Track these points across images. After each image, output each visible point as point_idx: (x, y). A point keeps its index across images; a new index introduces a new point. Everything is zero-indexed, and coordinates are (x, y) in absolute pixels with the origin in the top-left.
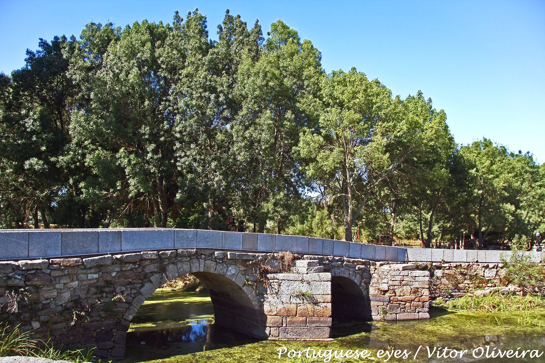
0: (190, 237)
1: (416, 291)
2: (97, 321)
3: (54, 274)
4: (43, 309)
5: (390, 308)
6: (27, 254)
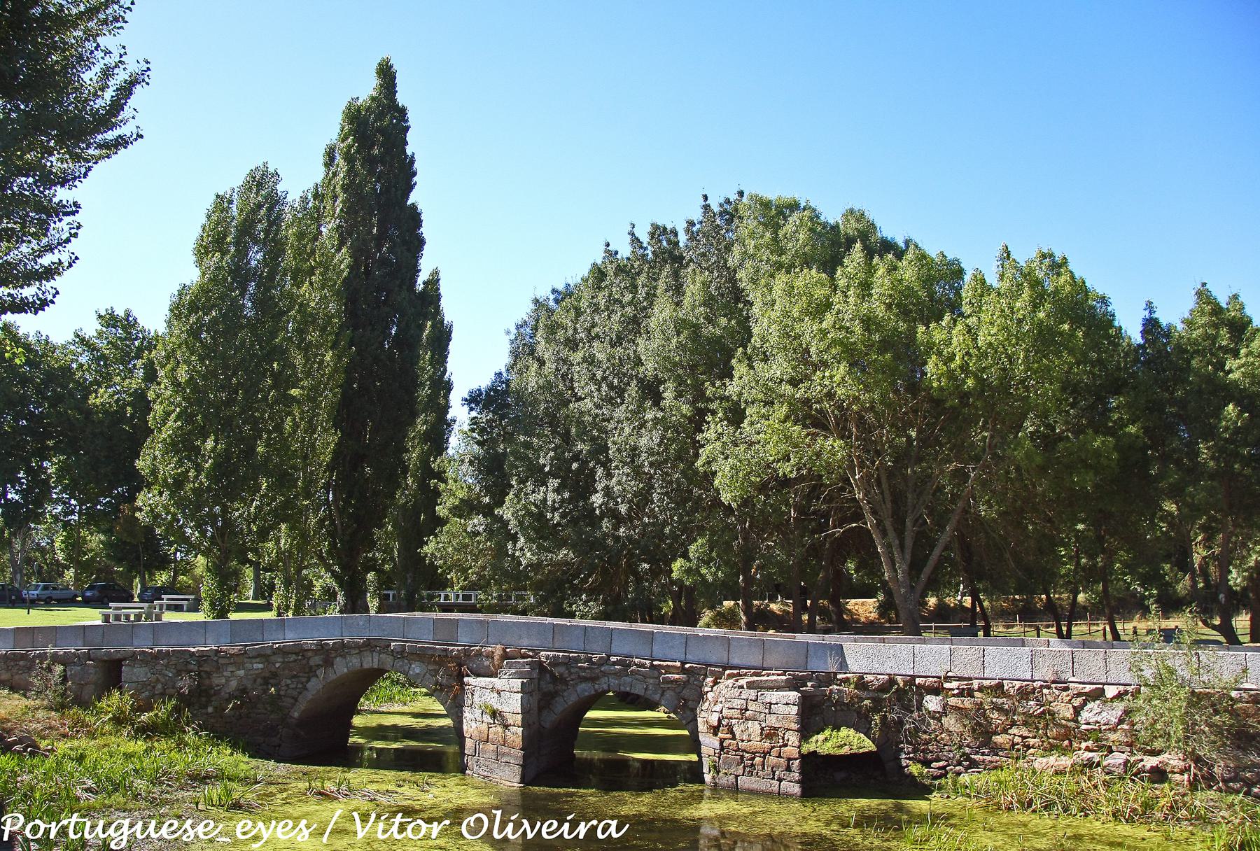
1: (770, 734)
3: (221, 661)
5: (724, 763)
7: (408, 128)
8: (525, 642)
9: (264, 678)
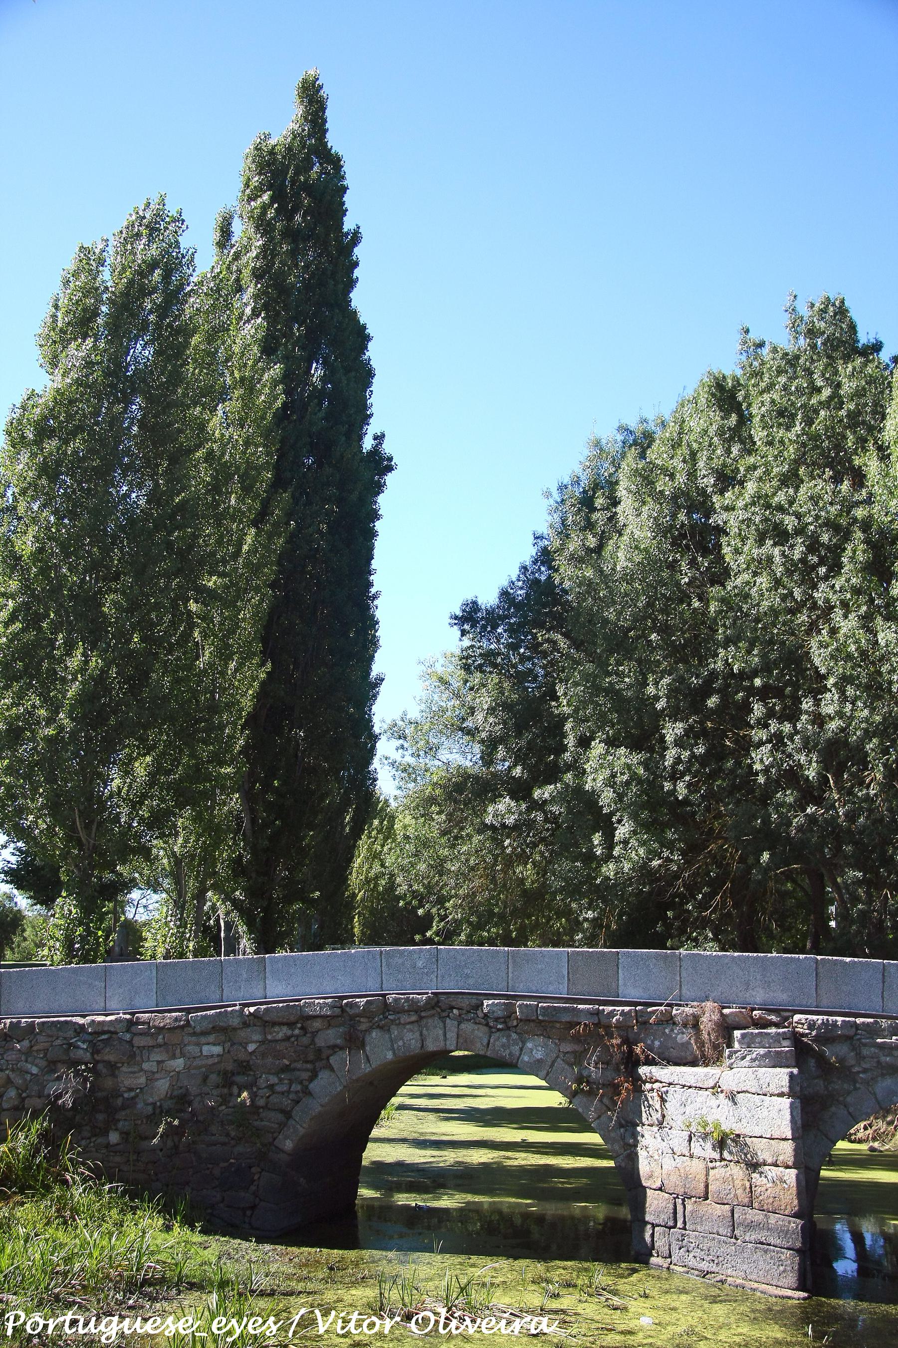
0: (420, 964)
2: (224, 1144)
3: (139, 1041)
4: (123, 1108)
6: (103, 1004)
7: (344, 189)
8: (759, 996)
9: (225, 1073)
